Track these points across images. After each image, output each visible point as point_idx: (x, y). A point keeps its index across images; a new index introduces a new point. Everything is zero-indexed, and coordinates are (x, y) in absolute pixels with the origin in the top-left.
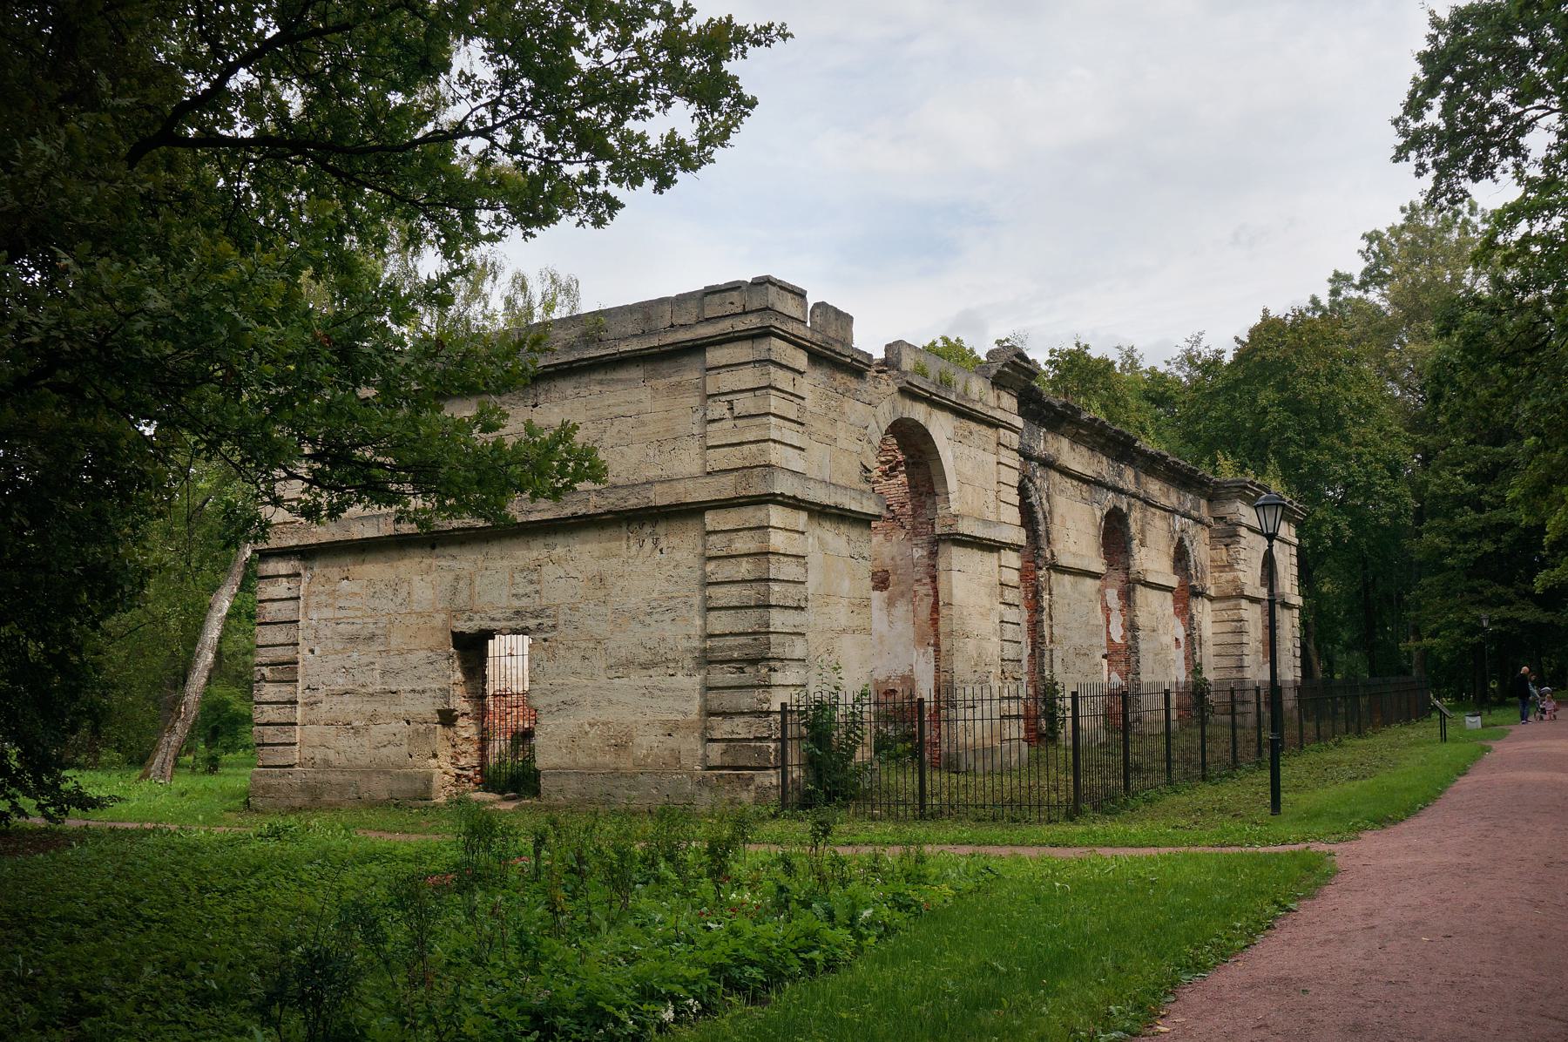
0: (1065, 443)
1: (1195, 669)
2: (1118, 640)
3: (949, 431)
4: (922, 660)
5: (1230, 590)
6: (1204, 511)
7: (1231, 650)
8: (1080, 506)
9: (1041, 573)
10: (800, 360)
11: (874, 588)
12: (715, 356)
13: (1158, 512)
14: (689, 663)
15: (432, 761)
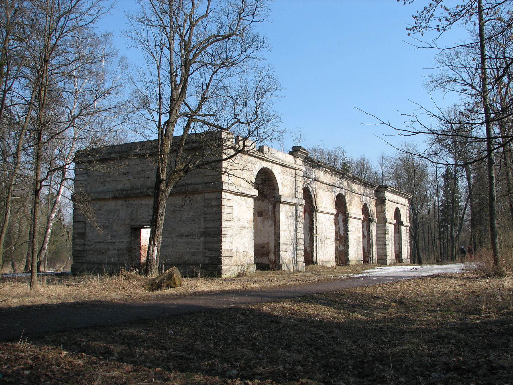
2: (342, 235)
3: (279, 171)
11: (259, 216)
13: (356, 195)
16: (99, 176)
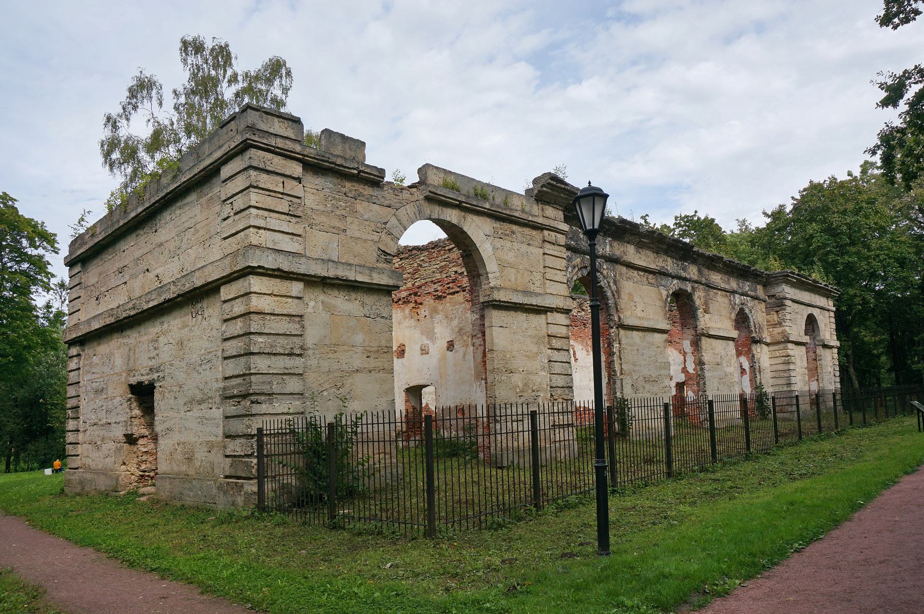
0: (631, 249)
1: (757, 387)
2: (691, 371)
4: (479, 390)
5: (780, 338)
6: (760, 291)
7: (782, 374)
8: (646, 288)
9: (612, 330)
10: (296, 169)
12: (226, 171)
13: (719, 292)
14: (218, 399)
15: (124, 467)
16: (93, 285)
